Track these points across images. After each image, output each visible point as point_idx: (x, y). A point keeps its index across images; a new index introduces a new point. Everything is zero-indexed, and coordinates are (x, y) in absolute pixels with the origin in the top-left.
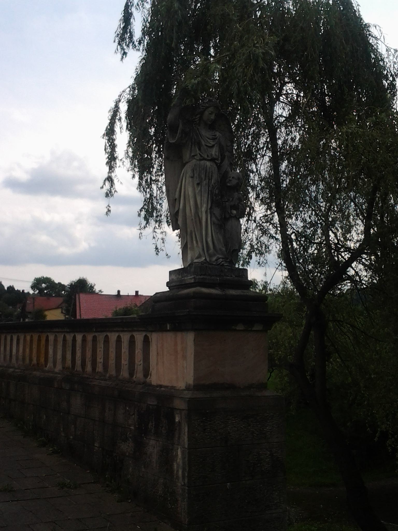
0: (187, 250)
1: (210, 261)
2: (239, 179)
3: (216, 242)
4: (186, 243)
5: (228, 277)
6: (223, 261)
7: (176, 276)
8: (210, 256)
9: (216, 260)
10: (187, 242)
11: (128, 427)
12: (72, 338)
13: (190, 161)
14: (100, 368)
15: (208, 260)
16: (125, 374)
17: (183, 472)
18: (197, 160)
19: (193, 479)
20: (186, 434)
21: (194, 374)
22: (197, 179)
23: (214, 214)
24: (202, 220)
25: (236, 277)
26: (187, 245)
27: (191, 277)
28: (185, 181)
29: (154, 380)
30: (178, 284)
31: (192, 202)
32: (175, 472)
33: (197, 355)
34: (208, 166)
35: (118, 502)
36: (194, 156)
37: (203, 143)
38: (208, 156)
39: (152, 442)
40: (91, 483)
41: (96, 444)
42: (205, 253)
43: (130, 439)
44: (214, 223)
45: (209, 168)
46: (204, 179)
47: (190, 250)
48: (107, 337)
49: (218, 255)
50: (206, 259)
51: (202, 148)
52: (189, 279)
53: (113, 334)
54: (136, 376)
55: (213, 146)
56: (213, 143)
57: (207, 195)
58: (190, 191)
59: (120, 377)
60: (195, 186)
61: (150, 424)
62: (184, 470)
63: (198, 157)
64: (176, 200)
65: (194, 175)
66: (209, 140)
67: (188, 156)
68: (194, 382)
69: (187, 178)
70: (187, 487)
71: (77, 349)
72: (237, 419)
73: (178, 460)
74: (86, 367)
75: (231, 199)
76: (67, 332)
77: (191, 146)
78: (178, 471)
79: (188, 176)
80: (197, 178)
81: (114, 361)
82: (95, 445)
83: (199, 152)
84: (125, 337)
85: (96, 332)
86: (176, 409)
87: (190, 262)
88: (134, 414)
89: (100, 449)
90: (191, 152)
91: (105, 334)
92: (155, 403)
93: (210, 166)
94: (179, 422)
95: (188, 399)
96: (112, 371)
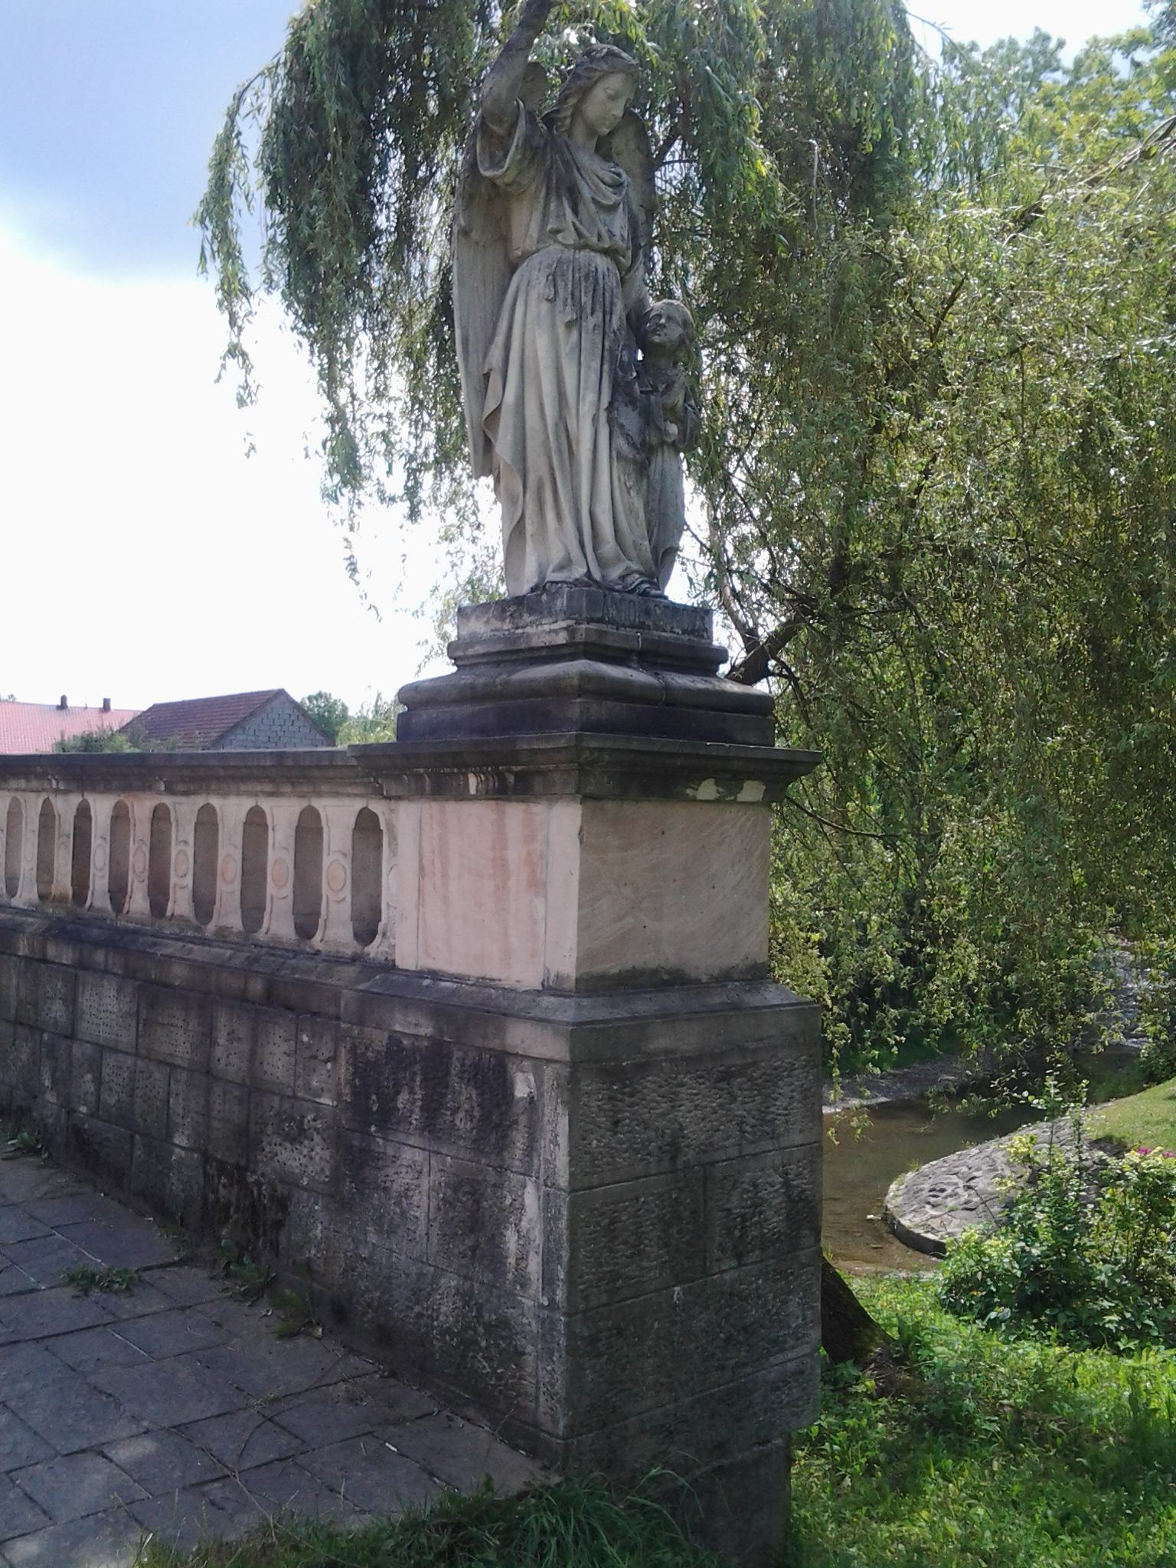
2: (685, 324)
3: (622, 518)
4: (519, 522)
5: (664, 634)
6: (642, 583)
7: (487, 622)
9: (623, 578)
10: (523, 517)
11: (308, 1097)
12: (74, 811)
13: (538, 251)
14: (180, 903)
15: (597, 575)
16: (279, 925)
17: (545, 1263)
18: (567, 246)
19: (582, 1287)
20: (563, 1140)
21: (579, 943)
22: (568, 308)
23: (622, 426)
25: (684, 632)
27: (554, 627)
29: (407, 958)
30: (498, 648)
32: (512, 1260)
33: (588, 882)
35: (281, 1337)
37: (586, 193)
38: (600, 237)
39: (408, 1155)
40: (173, 1264)
41: (180, 1140)
43: (317, 1138)
44: (620, 457)
47: (534, 543)
48: (208, 811)
49: (630, 563)
50: (589, 574)
51: (581, 208)
52: (548, 631)
53: (31, 796)
54: (323, 935)
56: (614, 198)
57: (599, 362)
58: (542, 345)
59: (261, 936)
60: (561, 329)
61: (403, 1098)
62: (549, 1259)
65: (556, 292)
66: (603, 186)
67: (534, 231)
68: (578, 969)
69: (533, 302)
70: (565, 1314)
71: (95, 842)
72: (703, 1083)
73: (524, 1224)
74: (127, 899)
75: (662, 387)
76: (57, 791)
78: (522, 1258)
79: (534, 294)
80: (565, 305)
81: (236, 887)
82: (177, 1141)
83: (575, 220)
84: (33, 805)
85: (170, 791)
86: (516, 1055)
88: (334, 1059)
89: (196, 1155)
91: (199, 801)
92: (426, 1029)
94: (531, 1099)
95: (570, 1028)
96: (229, 915)
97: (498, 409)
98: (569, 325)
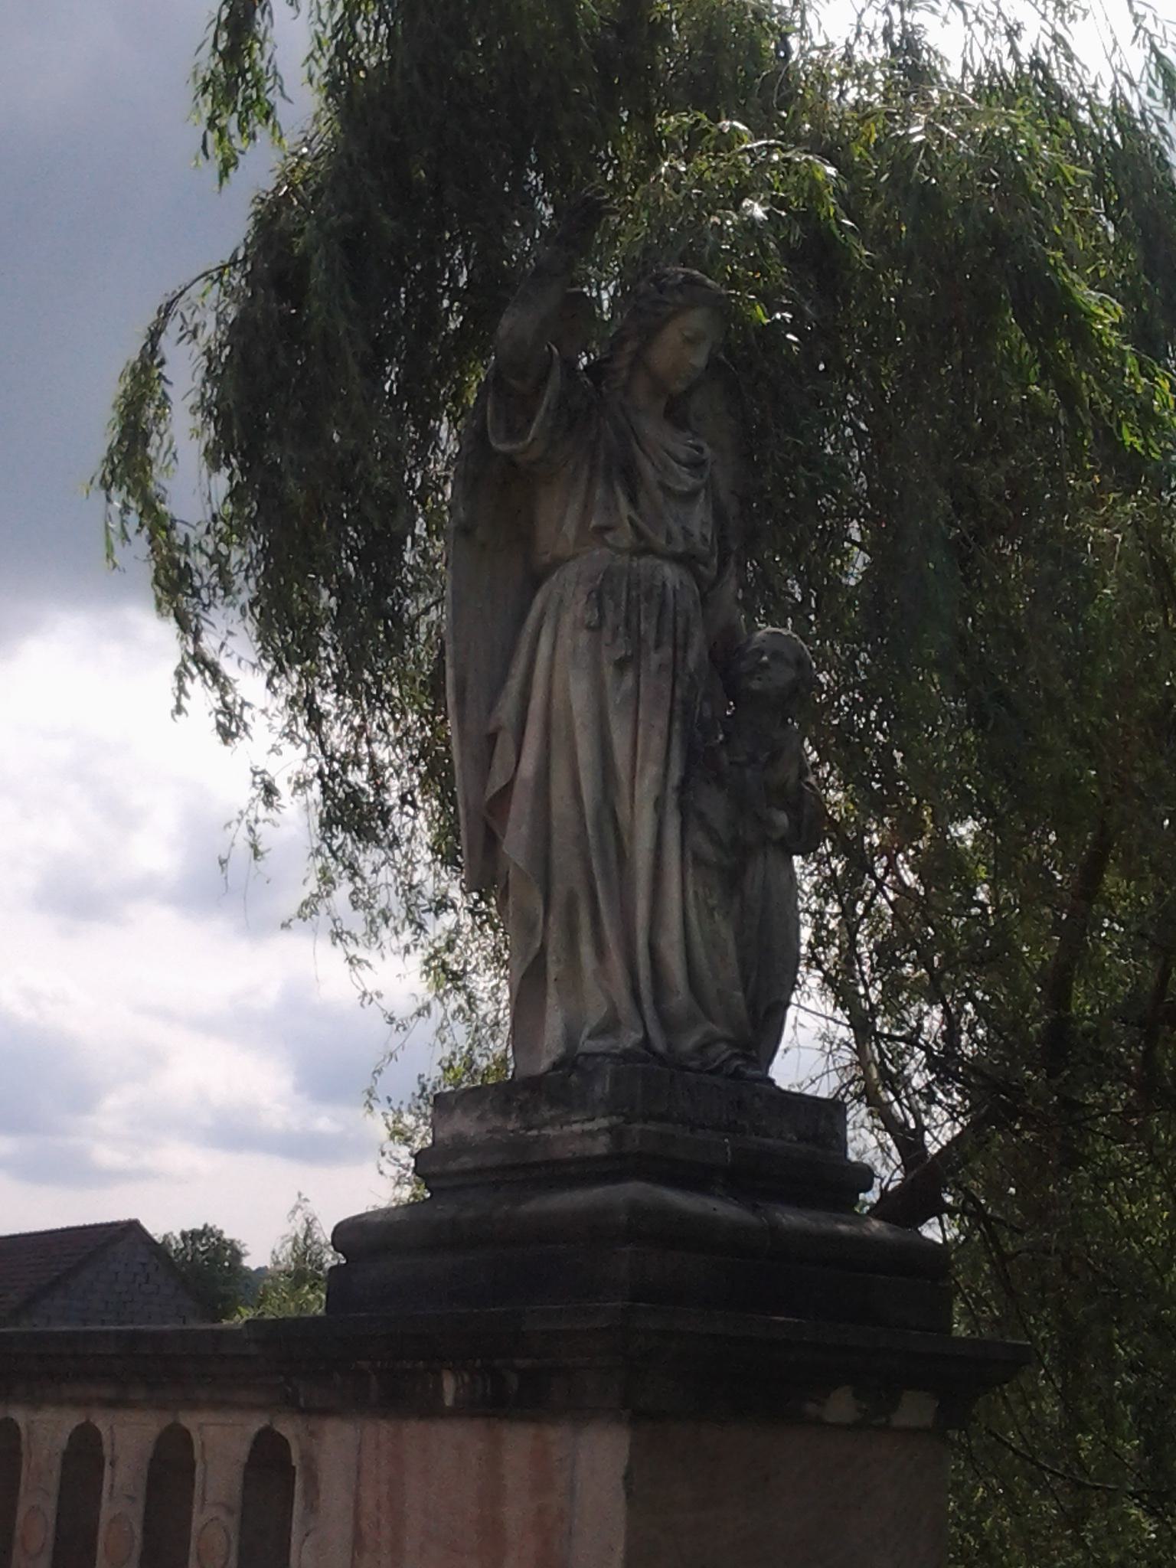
0: (544, 995)
1: (670, 1048)
5: (769, 1141)
8: (667, 1024)
9: (701, 1048)
10: (543, 949)
13: (574, 557)
15: (659, 1044)
23: (701, 815)
24: (632, 837)
26: (545, 966)
28: (554, 648)
31: (586, 753)
34: (669, 585)
36: (602, 530)
38: (670, 538)
42: (642, 1017)
45: (675, 591)
46: (651, 643)
50: (646, 1041)
55: (690, 496)
58: (578, 691)
60: (609, 671)
63: (625, 537)
64: (492, 738)
65: (602, 617)
67: (570, 529)
69: (566, 629)
77: (590, 480)
79: (567, 619)
80: (615, 635)
83: (632, 513)
87: (561, 1050)
90: (587, 509)
93: (678, 587)
97: (507, 789)
98: (621, 665)
